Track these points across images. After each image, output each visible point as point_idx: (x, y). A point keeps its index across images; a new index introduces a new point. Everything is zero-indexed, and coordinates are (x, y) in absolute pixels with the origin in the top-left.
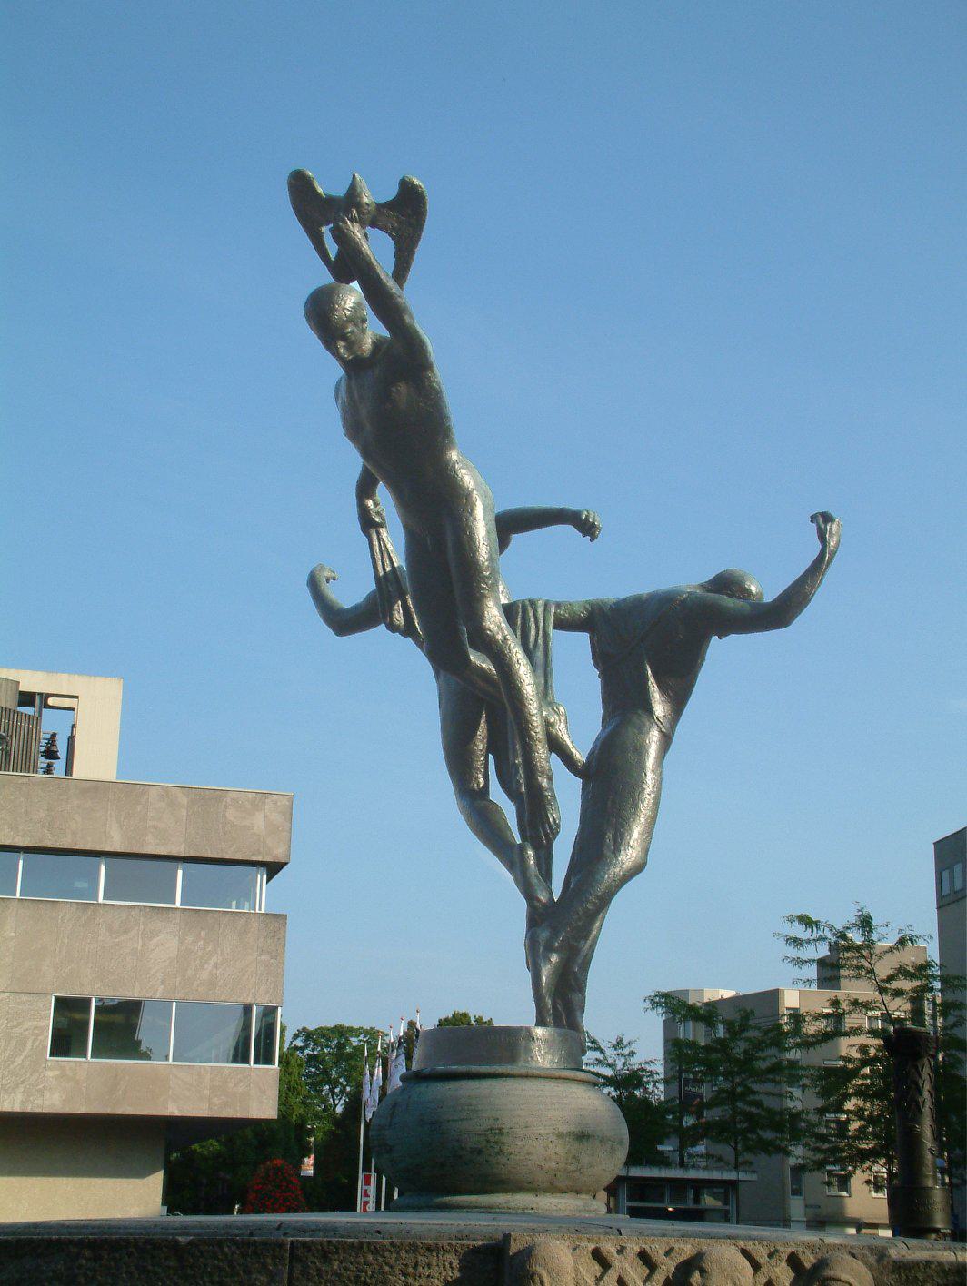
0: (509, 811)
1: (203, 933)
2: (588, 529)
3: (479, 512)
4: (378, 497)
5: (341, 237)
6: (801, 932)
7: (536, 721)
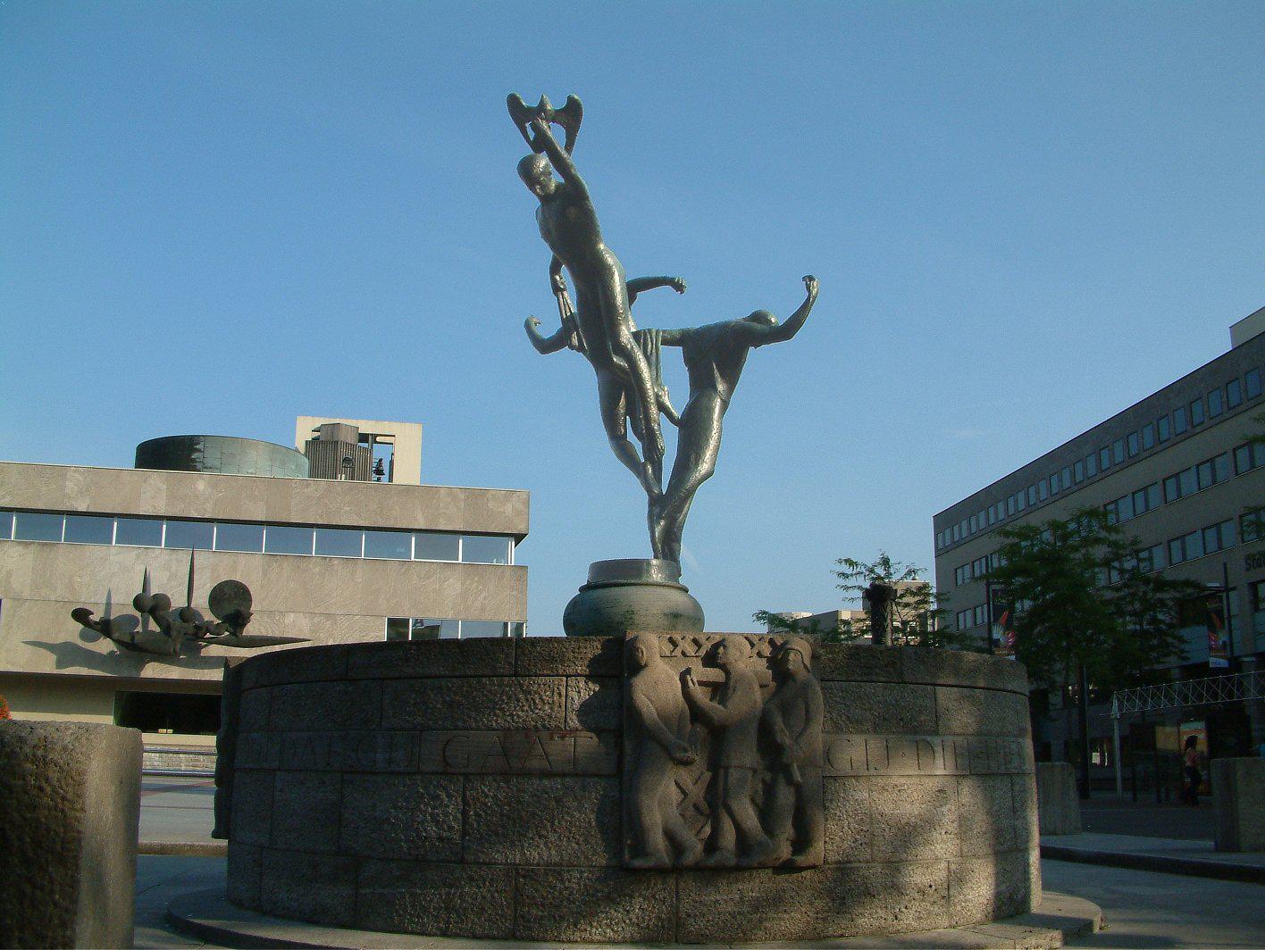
0: (637, 446)
1: (476, 579)
2: (679, 287)
3: (616, 274)
4: (562, 274)
5: (536, 128)
6: (849, 570)
7: (650, 393)
